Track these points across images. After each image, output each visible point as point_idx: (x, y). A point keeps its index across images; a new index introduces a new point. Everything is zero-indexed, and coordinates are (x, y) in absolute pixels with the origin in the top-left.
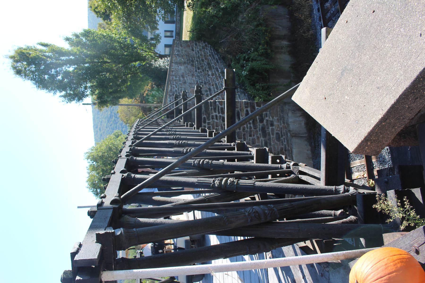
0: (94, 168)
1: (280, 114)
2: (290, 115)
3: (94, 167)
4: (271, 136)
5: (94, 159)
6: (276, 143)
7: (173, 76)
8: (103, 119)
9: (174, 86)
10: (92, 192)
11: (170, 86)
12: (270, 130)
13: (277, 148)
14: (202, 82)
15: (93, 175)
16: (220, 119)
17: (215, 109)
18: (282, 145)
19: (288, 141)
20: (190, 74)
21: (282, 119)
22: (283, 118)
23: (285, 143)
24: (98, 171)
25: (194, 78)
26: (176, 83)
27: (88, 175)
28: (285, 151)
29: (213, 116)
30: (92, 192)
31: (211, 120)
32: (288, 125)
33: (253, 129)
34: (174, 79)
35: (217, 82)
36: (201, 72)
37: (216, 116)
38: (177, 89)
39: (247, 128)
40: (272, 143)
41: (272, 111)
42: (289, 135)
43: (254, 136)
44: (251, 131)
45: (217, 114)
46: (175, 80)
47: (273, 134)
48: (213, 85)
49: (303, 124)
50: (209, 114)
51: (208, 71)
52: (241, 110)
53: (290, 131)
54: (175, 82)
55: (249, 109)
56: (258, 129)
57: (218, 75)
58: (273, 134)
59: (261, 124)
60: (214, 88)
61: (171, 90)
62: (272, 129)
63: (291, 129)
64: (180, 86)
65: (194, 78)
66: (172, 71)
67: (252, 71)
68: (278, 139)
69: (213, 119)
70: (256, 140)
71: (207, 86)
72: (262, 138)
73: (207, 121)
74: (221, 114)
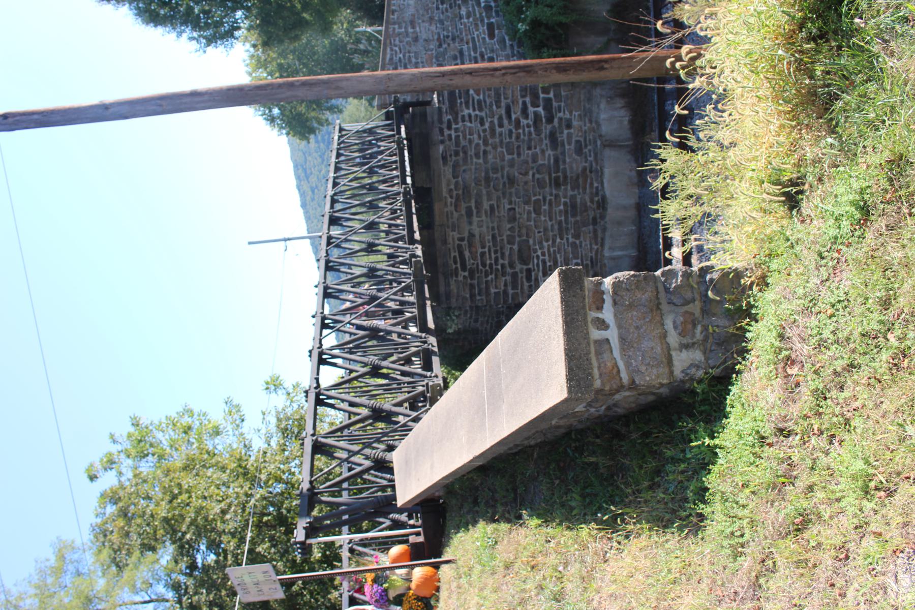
1: (584, 106)
2: (603, 106)
4: (567, 147)
6: (574, 159)
7: (394, 23)
9: (397, 49)
11: (388, 50)
12: (565, 136)
13: (575, 169)
14: (448, 37)
16: (476, 121)
17: (467, 103)
18: (586, 162)
19: (596, 155)
20: (426, 18)
21: (587, 115)
22: (591, 111)
23: (591, 159)
25: (433, 28)
26: (400, 41)
28: (591, 172)
29: (463, 116)
31: (461, 124)
32: (598, 125)
33: (534, 136)
34: (397, 31)
35: (476, 33)
36: (447, 10)
37: (470, 116)
38: (401, 56)
39: (524, 135)
40: (568, 160)
41: (569, 102)
42: (599, 143)
43: (535, 148)
44: (530, 140)
45: (471, 111)
46: (399, 34)
47: (569, 144)
48: (467, 43)
49: (626, 123)
50: (457, 114)
51: (460, 8)
52: (513, 103)
53: (600, 136)
54: (397, 39)
55: (528, 99)
56: (543, 136)
57: (478, 16)
58: (569, 144)
59: (549, 127)
60: (469, 48)
61: (391, 59)
62: (568, 134)
63: (603, 133)
64: (407, 47)
65: (433, 28)
66: (393, 12)
67: (536, 24)
68: (579, 150)
69: (463, 121)
70: (540, 156)
71: (457, 44)
72: (550, 152)
73: (454, 126)
74: (477, 112)
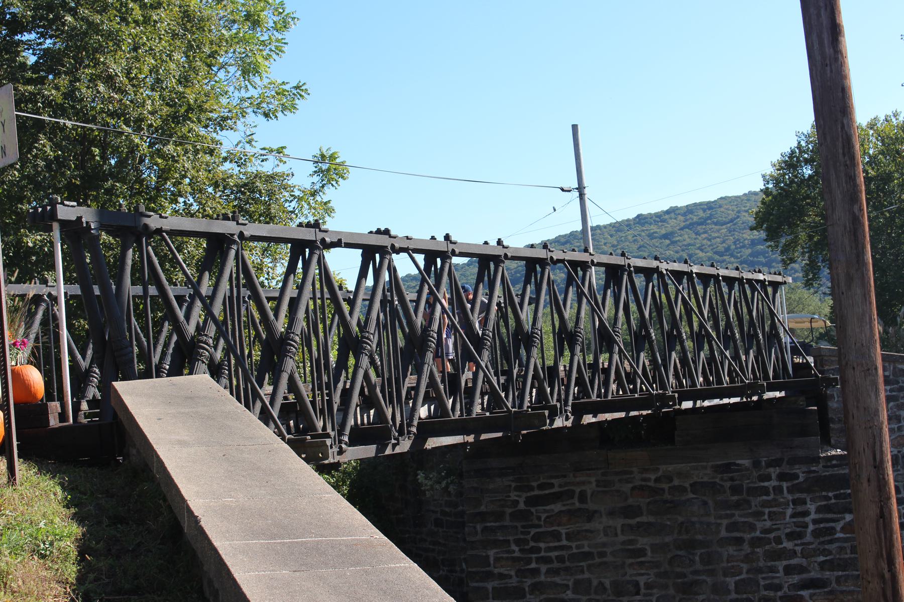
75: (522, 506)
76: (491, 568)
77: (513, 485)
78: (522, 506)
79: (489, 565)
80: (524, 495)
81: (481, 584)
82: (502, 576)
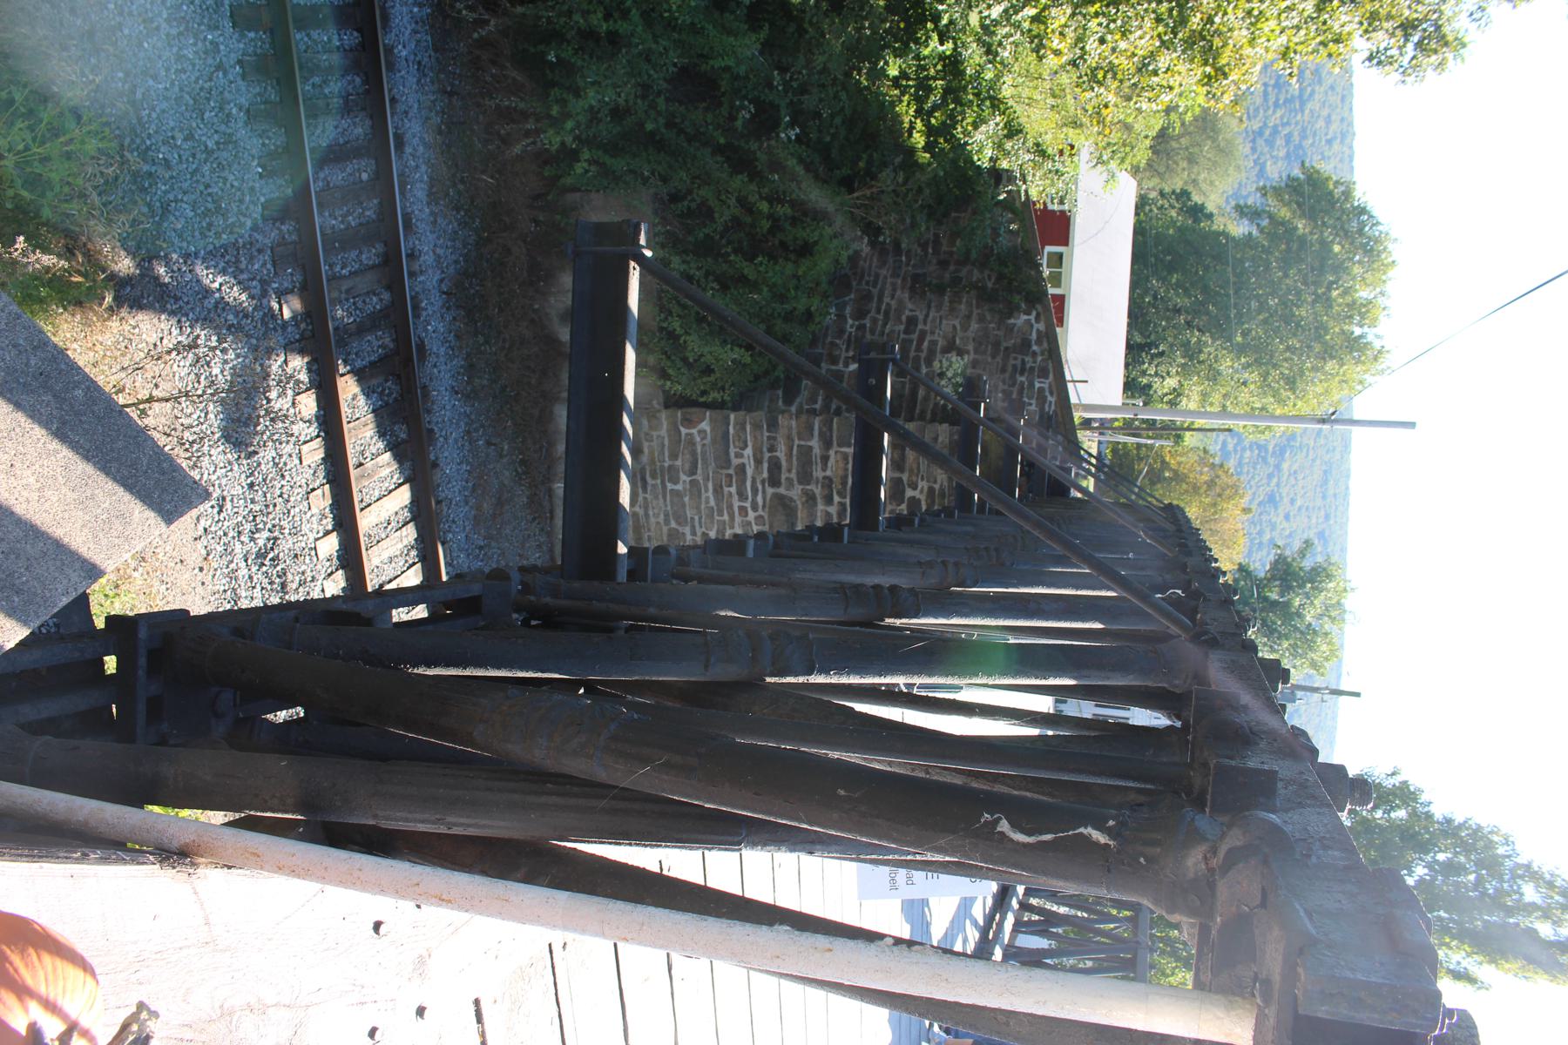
0: (1362, 311)
3: (1362, 316)
5: (1355, 346)
8: (1312, 443)
10: (1378, 223)
15: (1373, 285)
24: (1349, 299)
27: (1389, 288)
30: (1378, 223)
75: (909, 493)
76: (835, 447)
77: (937, 487)
78: (909, 493)
79: (839, 445)
80: (923, 498)
81: (816, 433)
82: (825, 459)
